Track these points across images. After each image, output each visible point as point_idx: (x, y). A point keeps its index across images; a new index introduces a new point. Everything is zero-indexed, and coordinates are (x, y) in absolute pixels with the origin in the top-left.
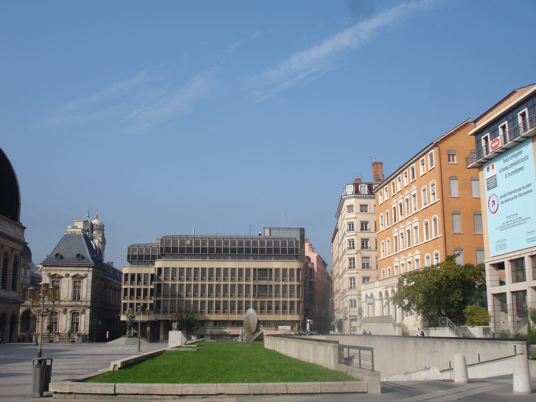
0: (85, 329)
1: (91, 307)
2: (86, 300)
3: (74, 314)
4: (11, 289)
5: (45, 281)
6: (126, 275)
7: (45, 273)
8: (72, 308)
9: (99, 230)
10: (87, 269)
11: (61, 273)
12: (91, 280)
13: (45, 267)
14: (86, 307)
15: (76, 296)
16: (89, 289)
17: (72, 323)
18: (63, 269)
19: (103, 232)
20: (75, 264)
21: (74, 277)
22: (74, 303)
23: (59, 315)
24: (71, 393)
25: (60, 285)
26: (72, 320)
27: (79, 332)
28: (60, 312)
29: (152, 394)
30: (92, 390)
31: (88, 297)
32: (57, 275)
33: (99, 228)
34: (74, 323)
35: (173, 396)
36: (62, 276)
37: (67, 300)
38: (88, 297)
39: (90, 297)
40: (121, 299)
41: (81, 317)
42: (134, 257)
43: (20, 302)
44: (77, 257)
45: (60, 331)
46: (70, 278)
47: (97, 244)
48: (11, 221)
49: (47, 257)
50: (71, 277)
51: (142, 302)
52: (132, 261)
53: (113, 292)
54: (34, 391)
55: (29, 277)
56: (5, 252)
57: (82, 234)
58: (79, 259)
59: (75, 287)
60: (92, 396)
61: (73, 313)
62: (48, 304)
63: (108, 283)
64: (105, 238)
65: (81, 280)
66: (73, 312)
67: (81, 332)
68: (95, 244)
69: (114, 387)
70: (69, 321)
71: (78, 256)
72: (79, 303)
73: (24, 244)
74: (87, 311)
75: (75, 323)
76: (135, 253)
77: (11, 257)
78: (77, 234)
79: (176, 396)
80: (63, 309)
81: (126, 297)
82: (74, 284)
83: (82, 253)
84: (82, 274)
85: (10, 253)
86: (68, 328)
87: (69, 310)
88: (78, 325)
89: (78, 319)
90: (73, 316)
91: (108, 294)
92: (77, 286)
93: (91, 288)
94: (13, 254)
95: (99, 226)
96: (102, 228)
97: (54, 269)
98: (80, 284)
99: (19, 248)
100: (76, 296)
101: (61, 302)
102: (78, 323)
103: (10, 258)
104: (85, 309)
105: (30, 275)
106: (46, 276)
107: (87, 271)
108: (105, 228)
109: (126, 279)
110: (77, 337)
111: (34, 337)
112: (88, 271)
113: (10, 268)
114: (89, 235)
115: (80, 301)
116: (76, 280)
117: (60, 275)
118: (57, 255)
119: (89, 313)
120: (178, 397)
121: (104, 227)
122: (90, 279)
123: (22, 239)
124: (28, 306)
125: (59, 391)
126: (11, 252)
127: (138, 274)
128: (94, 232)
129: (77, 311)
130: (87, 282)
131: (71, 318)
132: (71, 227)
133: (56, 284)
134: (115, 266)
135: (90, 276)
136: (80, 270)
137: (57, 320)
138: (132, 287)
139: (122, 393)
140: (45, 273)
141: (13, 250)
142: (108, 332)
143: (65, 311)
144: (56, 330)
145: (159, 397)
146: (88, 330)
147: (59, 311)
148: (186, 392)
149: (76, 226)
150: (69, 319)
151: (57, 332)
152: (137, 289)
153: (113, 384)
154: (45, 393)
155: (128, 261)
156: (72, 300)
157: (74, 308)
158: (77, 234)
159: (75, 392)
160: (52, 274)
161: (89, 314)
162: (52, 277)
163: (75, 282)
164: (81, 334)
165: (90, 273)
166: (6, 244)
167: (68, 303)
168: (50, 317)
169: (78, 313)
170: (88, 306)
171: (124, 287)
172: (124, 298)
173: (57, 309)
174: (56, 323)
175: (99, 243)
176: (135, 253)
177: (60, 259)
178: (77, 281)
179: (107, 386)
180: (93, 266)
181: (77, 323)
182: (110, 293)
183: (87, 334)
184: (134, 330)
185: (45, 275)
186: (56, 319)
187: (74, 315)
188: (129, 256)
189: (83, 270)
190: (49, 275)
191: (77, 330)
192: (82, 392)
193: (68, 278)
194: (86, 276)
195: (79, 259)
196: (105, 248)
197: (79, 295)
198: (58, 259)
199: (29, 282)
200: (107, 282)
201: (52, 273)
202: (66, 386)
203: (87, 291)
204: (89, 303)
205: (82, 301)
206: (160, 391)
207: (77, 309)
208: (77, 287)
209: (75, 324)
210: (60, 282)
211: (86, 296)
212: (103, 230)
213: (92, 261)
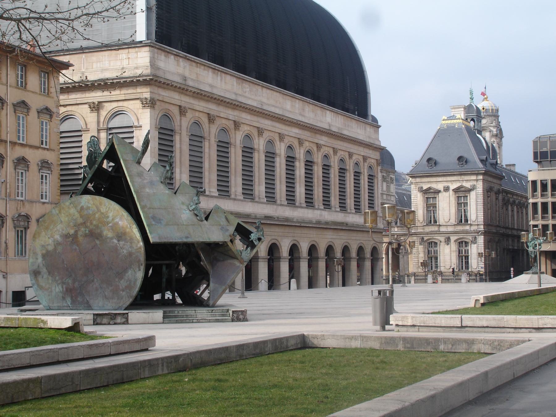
0: (478, 264)
1: (485, 233)
2: (477, 224)
3: (462, 243)
4: (338, 210)
5: (416, 198)
6: (534, 183)
7: (414, 188)
8: (458, 235)
9: (491, 117)
10: (474, 177)
11: (437, 186)
12: (482, 194)
13: (414, 179)
14: (478, 233)
15: (463, 219)
16: (480, 207)
17: (460, 257)
18: (439, 180)
19: (497, 120)
20: (457, 172)
21: (456, 190)
22: (459, 228)
23: (439, 246)
24: (414, 326)
25: (437, 203)
26: (459, 253)
27: (470, 270)
28: (441, 242)
29: (504, 327)
30: (437, 322)
31: (480, 218)
32: (431, 189)
33: (491, 114)
34: (462, 257)
35: (528, 329)
36: (440, 190)
37: (449, 224)
38: (480, 218)
39: (483, 218)
40: (529, 220)
41: (472, 247)
42: (544, 155)
43: (381, 231)
44: (459, 161)
45: (443, 269)
46: (451, 192)
47: (488, 139)
48: (359, 119)
49: (416, 164)
50: (453, 190)
51: (540, 222)
52: (541, 162)
53: (518, 209)
54: (375, 324)
55: (394, 194)
56: (355, 162)
57: (463, 126)
58: (462, 164)
59: (459, 204)
60: (437, 328)
61: (460, 243)
62: (422, 231)
63: (509, 195)
64: (502, 127)
65: (467, 195)
66: (459, 241)
67: (473, 270)
68: (484, 139)
69: (460, 319)
70: (455, 254)
71: (460, 158)
72: (467, 228)
73: (380, 149)
74: (479, 239)
75: (464, 257)
76: (544, 149)
77: (364, 169)
78: (457, 126)
79: (532, 329)
80: (444, 237)
81: (535, 216)
82: (427, 201)
83: (465, 155)
84: (468, 185)
85: (362, 163)
86: (454, 264)
87: (453, 238)
88: (468, 259)
89: (467, 251)
90: (460, 247)
91: (510, 212)
92: (462, 203)
93: (482, 205)
94: (366, 164)
95: (490, 110)
96: (495, 112)
97: (426, 181)
98: (467, 200)
99: (375, 155)
100: (463, 219)
101: (440, 227)
102: (468, 257)
103: (362, 171)
104: (477, 237)
105: (396, 192)
106: (416, 192)
107: (474, 180)
108: (499, 113)
109: (534, 190)
110: (468, 278)
111: (406, 278)
112: (477, 180)
113: (364, 184)
114: (474, 126)
115: (469, 225)
116: (460, 195)
117: (437, 188)
118: (429, 160)
119: (483, 241)
120: (534, 330)
121: (498, 111)
122: (480, 191)
123: (377, 143)
124: (396, 236)
125: (400, 323)
126: (364, 162)
127: (541, 181)
128: (484, 121)
129: (465, 240)
130: (477, 197)
131: (457, 250)
132: (446, 118)
133: (431, 201)
134: (518, 169)
135: (480, 187)
136: (465, 179)
137: (437, 253)
138: (544, 200)
139: (470, 326)
140: (414, 188)
141: (365, 159)
142: (512, 269)
143: (448, 241)
144: (437, 267)
145: (512, 330)
146: (483, 266)
147: (439, 240)
148: (543, 325)
149: (454, 116)
150: (454, 251)
151: (439, 270)
152: (552, 203)
153: (460, 316)
154: (387, 327)
155: (535, 162)
156: (456, 223)
157: (461, 236)
158: (457, 126)
159: (418, 325)
160: (424, 189)
161: (483, 243)
162: (424, 193)
163: (458, 197)
164: (472, 272)
165: (479, 183)
166: (355, 152)
167: (450, 229)
168: (427, 250)
169: (466, 243)
170: (480, 231)
171: (531, 201)
172: (534, 218)
173: (436, 237)
174: (436, 258)
175: (493, 136)
176: (544, 149)
177: (465, 163)
178: (461, 197)
179: (452, 317)
180: (484, 172)
181: (467, 257)
182: (513, 211)
183: (481, 273)
184: (553, 264)
185: (415, 190)
186: (436, 252)
187: (461, 245)
188: (535, 154)
189: (469, 179)
190: (421, 190)
191: (467, 268)
192: (425, 325)
193: (448, 193)
194: (473, 188)
195: (462, 164)
196: (502, 144)
197: (465, 216)
198: (431, 166)
199: (395, 202)
200: (507, 195)
201: (425, 187)
202: (408, 319)
203: (477, 210)
204: (482, 227)
205: (471, 225)
206: (512, 324)
207: (464, 237)
208: (462, 204)
209: (464, 259)
210: (437, 198)
211: (477, 217)
212: (498, 116)
213: (481, 165)
